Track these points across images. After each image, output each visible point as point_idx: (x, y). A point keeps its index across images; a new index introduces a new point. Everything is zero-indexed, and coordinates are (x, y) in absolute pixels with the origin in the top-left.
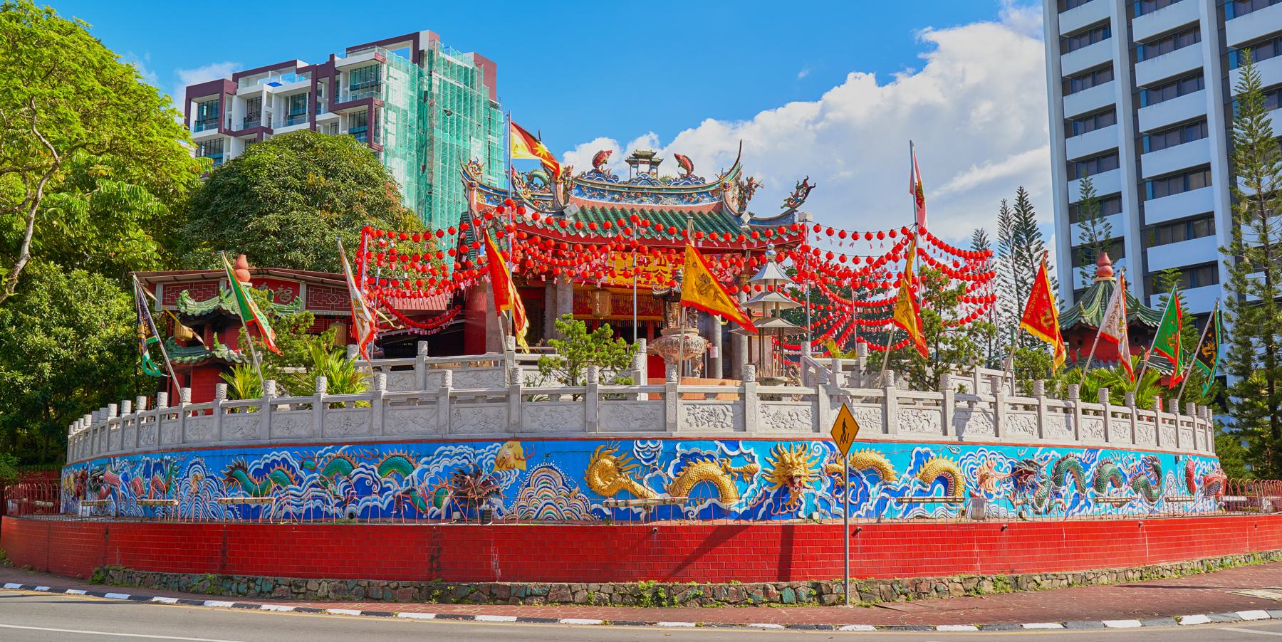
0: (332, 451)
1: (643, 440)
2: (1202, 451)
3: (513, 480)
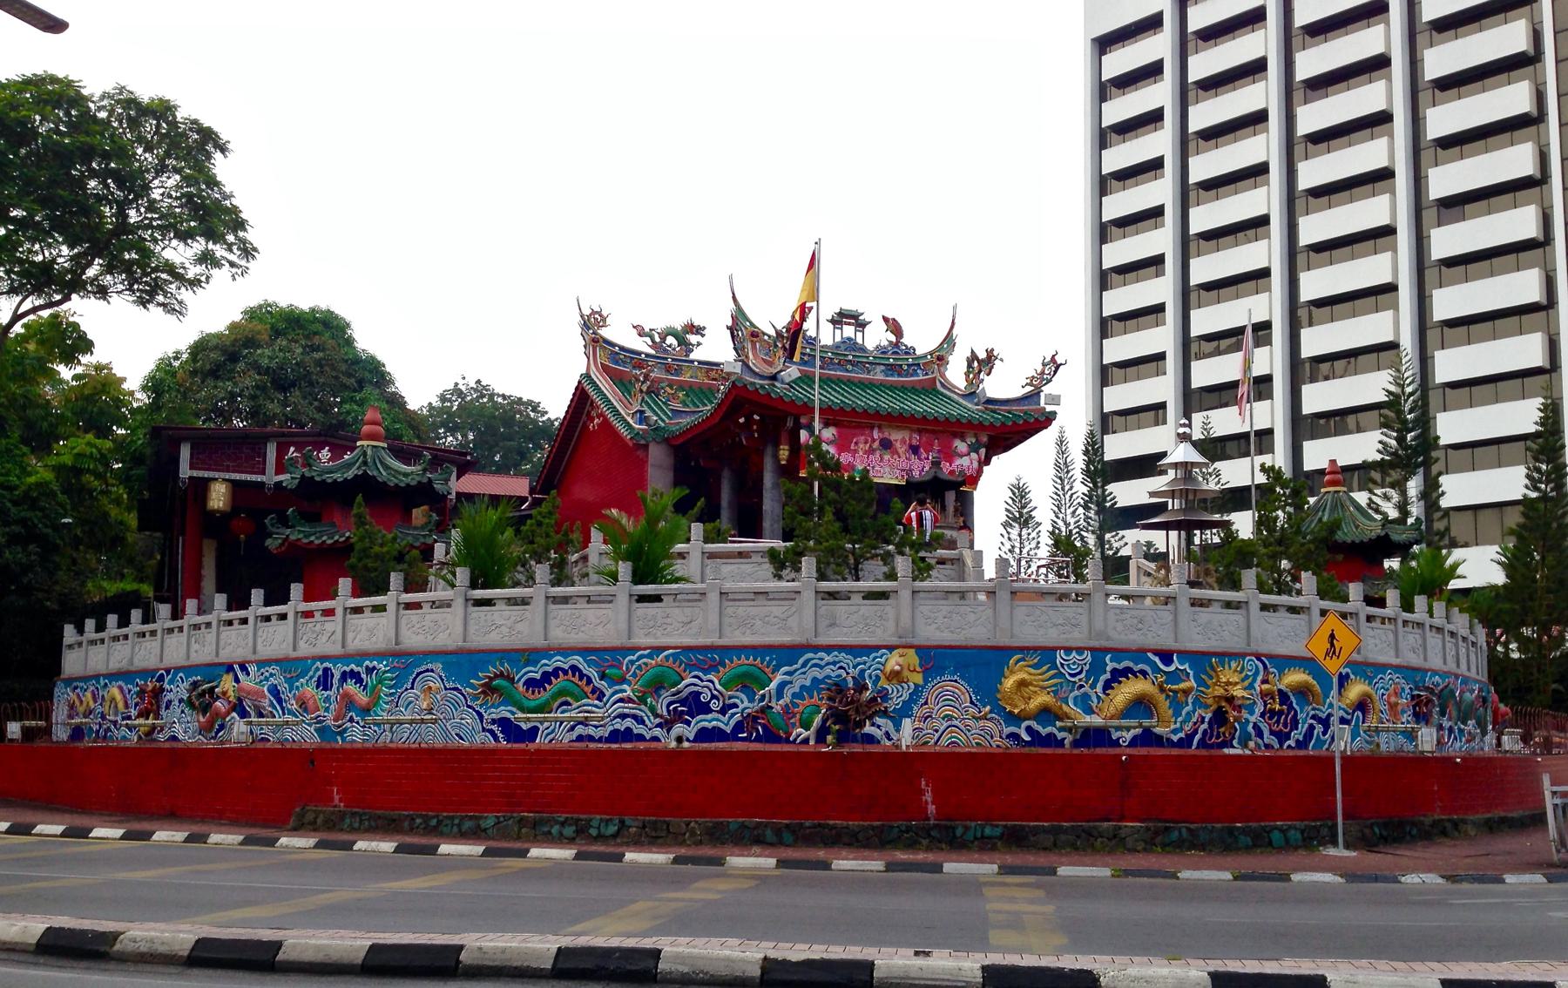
0: (650, 656)
1: (1068, 650)
2: (1473, 674)
3: (906, 696)
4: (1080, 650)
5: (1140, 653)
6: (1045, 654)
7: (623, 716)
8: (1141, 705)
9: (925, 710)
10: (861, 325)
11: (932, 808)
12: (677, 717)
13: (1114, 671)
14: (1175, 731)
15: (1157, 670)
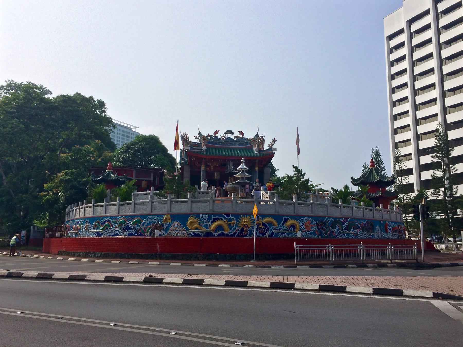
4: (206, 214)
5: (221, 215)
6: (197, 215)
7: (116, 231)
8: (220, 227)
9: (171, 228)
10: (232, 134)
11: (159, 250)
12: (125, 231)
13: (214, 219)
14: (230, 233)
15: (225, 218)
